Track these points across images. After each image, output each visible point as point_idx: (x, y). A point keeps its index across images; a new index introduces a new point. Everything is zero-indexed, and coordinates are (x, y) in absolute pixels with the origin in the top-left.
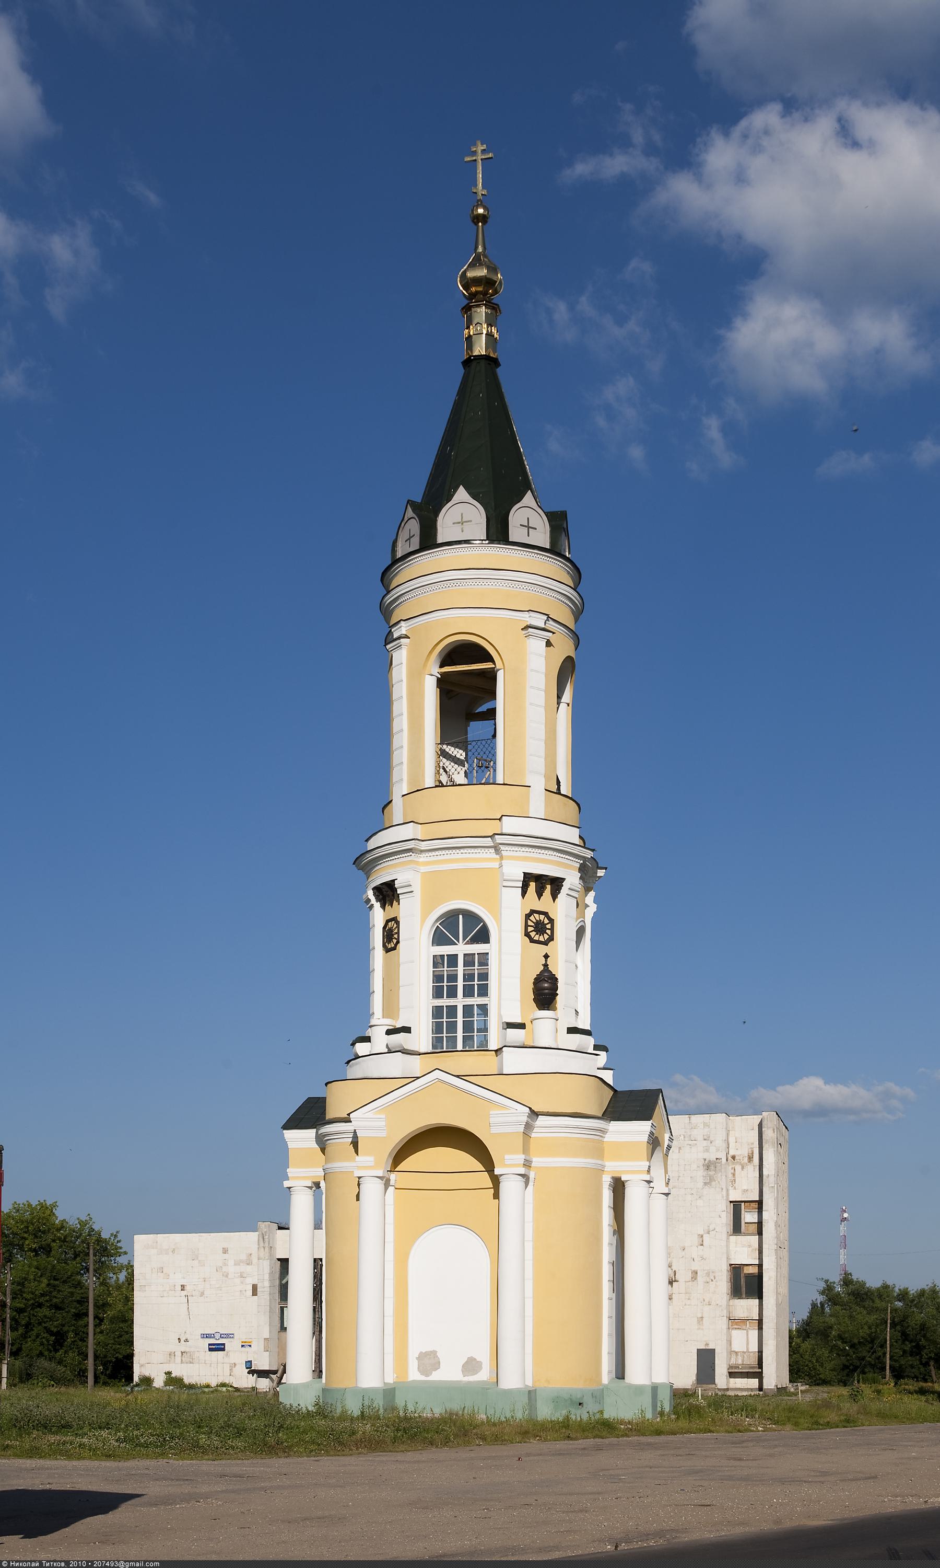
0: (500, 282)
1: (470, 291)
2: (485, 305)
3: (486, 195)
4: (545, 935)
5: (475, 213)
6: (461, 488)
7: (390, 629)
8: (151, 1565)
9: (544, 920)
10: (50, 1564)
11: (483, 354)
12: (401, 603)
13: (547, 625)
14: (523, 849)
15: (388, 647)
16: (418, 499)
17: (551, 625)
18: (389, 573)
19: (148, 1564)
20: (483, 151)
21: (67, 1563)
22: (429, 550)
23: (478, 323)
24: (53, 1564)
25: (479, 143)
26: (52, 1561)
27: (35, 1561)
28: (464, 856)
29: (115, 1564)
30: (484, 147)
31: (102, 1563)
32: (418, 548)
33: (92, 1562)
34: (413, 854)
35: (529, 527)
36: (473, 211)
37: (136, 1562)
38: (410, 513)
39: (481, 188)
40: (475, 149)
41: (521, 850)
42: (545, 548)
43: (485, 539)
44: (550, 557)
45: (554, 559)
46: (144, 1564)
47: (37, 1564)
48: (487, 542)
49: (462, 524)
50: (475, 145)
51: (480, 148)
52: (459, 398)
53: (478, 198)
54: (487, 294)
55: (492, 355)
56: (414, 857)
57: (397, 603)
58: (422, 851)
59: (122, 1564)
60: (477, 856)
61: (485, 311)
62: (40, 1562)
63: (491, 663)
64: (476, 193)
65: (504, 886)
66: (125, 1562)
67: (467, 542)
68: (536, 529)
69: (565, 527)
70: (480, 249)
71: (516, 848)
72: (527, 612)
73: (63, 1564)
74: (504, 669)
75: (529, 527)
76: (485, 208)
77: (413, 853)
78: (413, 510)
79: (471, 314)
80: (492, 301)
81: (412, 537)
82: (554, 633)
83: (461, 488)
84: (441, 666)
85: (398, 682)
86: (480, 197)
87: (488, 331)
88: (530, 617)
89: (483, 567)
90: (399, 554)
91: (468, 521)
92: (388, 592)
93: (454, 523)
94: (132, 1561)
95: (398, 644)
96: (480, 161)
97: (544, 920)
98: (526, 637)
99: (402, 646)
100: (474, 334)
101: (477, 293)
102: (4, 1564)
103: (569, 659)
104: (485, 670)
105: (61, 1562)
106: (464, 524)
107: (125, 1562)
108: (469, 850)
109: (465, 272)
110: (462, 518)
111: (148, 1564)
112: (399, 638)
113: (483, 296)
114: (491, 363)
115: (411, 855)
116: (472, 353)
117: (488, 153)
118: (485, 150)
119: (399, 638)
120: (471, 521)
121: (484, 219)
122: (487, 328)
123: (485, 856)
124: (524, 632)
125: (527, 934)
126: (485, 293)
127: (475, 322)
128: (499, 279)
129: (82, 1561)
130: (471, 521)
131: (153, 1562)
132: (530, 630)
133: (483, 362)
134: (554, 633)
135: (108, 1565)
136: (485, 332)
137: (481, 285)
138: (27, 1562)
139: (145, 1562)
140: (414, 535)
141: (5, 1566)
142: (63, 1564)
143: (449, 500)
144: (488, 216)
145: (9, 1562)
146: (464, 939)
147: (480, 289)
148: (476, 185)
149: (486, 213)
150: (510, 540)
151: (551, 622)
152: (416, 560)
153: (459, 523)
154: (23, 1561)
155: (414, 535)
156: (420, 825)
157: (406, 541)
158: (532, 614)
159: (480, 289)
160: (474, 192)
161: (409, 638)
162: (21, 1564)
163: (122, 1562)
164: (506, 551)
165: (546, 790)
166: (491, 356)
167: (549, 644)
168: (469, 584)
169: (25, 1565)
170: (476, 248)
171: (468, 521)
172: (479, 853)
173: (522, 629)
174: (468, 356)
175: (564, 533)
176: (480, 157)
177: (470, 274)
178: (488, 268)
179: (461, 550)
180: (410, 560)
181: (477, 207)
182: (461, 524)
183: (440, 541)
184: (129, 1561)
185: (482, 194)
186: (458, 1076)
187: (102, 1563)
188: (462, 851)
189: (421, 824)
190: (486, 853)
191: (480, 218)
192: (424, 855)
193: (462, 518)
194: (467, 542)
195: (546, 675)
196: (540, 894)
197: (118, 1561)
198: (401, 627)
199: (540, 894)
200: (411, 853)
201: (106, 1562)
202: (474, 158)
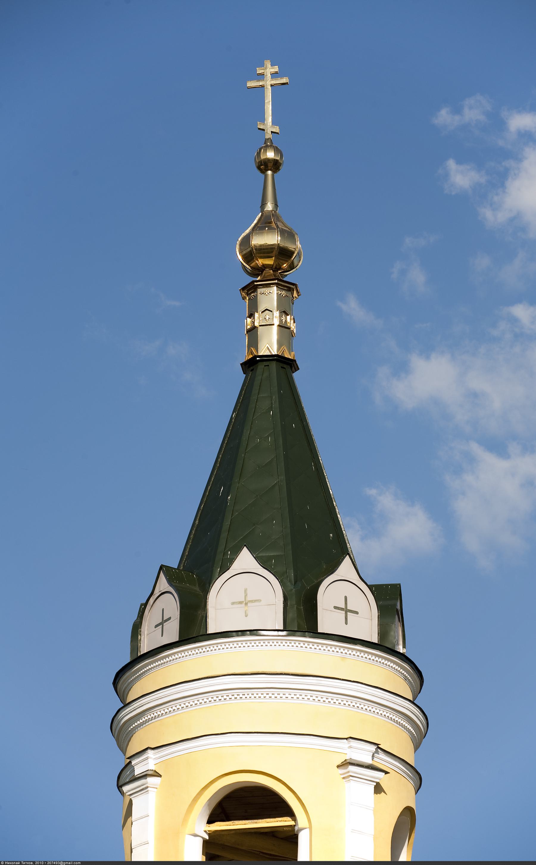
0: (299, 254)
1: (253, 264)
2: (277, 285)
3: (278, 133)
5: (263, 157)
6: (245, 551)
7: (128, 760)
8: (77, 863)
11: (274, 354)
12: (146, 721)
13: (375, 759)
15: (125, 789)
16: (174, 563)
17: (382, 760)
18: (128, 674)
19: (75, 863)
20: (274, 75)
21: (34, 862)
22: (195, 642)
23: (267, 310)
24: (27, 863)
25: (268, 63)
26: (26, 862)
27: (18, 862)
29: (58, 863)
30: (276, 69)
31: (52, 863)
32: (177, 639)
33: (46, 862)
35: (347, 611)
36: (259, 154)
38: (163, 584)
39: (271, 124)
40: (261, 72)
42: (372, 643)
43: (282, 628)
44: (379, 657)
45: (386, 659)
46: (73, 863)
47: (19, 863)
48: (284, 633)
49: (246, 604)
50: (262, 65)
51: (269, 69)
52: (237, 415)
53: (267, 137)
54: (280, 268)
55: (287, 355)
57: (141, 721)
59: (61, 863)
61: (277, 293)
62: (20, 862)
63: (289, 819)
64: (263, 130)
67: (253, 632)
69: (399, 607)
70: (269, 207)
72: (345, 740)
73: (32, 863)
74: (310, 828)
75: (347, 611)
76: (277, 150)
78: (170, 581)
79: (256, 297)
80: (285, 279)
81: (166, 620)
82: (386, 773)
83: (245, 551)
84: (210, 821)
85: (141, 845)
86: (269, 135)
87: (281, 321)
88: (350, 747)
89: (279, 671)
90: (144, 649)
91: (255, 601)
92: (126, 705)
93: (233, 603)
96: (270, 87)
98: (344, 778)
99: (149, 789)
100: (260, 326)
101: (265, 267)
102: (2, 863)
103: (408, 812)
104: (278, 829)
105: (31, 862)
106: (249, 604)
109: (247, 239)
110: (246, 596)
111: (75, 863)
112: (144, 776)
113: (273, 271)
114: (285, 366)
116: (257, 351)
117: (282, 77)
118: (276, 73)
119: (144, 776)
120: (259, 601)
121: (275, 165)
122: (281, 316)
126: (276, 268)
127: (261, 308)
128: (297, 250)
129: (41, 862)
130: (259, 601)
132: (351, 768)
133: (274, 365)
134: (386, 773)
136: (276, 322)
137: (272, 257)
138: (13, 862)
139: (73, 862)
140: (170, 619)
142: (32, 863)
143: (225, 568)
144: (281, 162)
145: (4, 862)
147: (270, 262)
148: (263, 120)
149: (278, 158)
150: (319, 631)
151: (382, 755)
152: (173, 657)
153: (241, 603)
154: (12, 862)
155: (170, 619)
157: (156, 626)
158: (354, 743)
159: (270, 262)
160: (259, 129)
161: (160, 776)
163: (62, 862)
164: (308, 647)
166: (286, 356)
167: (378, 789)
168: (257, 696)
169: (13, 863)
170: (263, 204)
171: (255, 601)
173: (338, 767)
174: (251, 356)
175: (397, 616)
176: (268, 82)
177: (258, 241)
178: (283, 233)
179: (240, 645)
180: (165, 657)
181: (266, 147)
182: (243, 605)
183: (211, 630)
184: (65, 862)
185: (272, 132)
187: (52, 863)
190: (249, 646)
191: (270, 165)
193: (246, 596)
194: (253, 632)
195: (375, 838)
197: (60, 862)
198: (147, 759)
201: (54, 862)
202: (261, 83)
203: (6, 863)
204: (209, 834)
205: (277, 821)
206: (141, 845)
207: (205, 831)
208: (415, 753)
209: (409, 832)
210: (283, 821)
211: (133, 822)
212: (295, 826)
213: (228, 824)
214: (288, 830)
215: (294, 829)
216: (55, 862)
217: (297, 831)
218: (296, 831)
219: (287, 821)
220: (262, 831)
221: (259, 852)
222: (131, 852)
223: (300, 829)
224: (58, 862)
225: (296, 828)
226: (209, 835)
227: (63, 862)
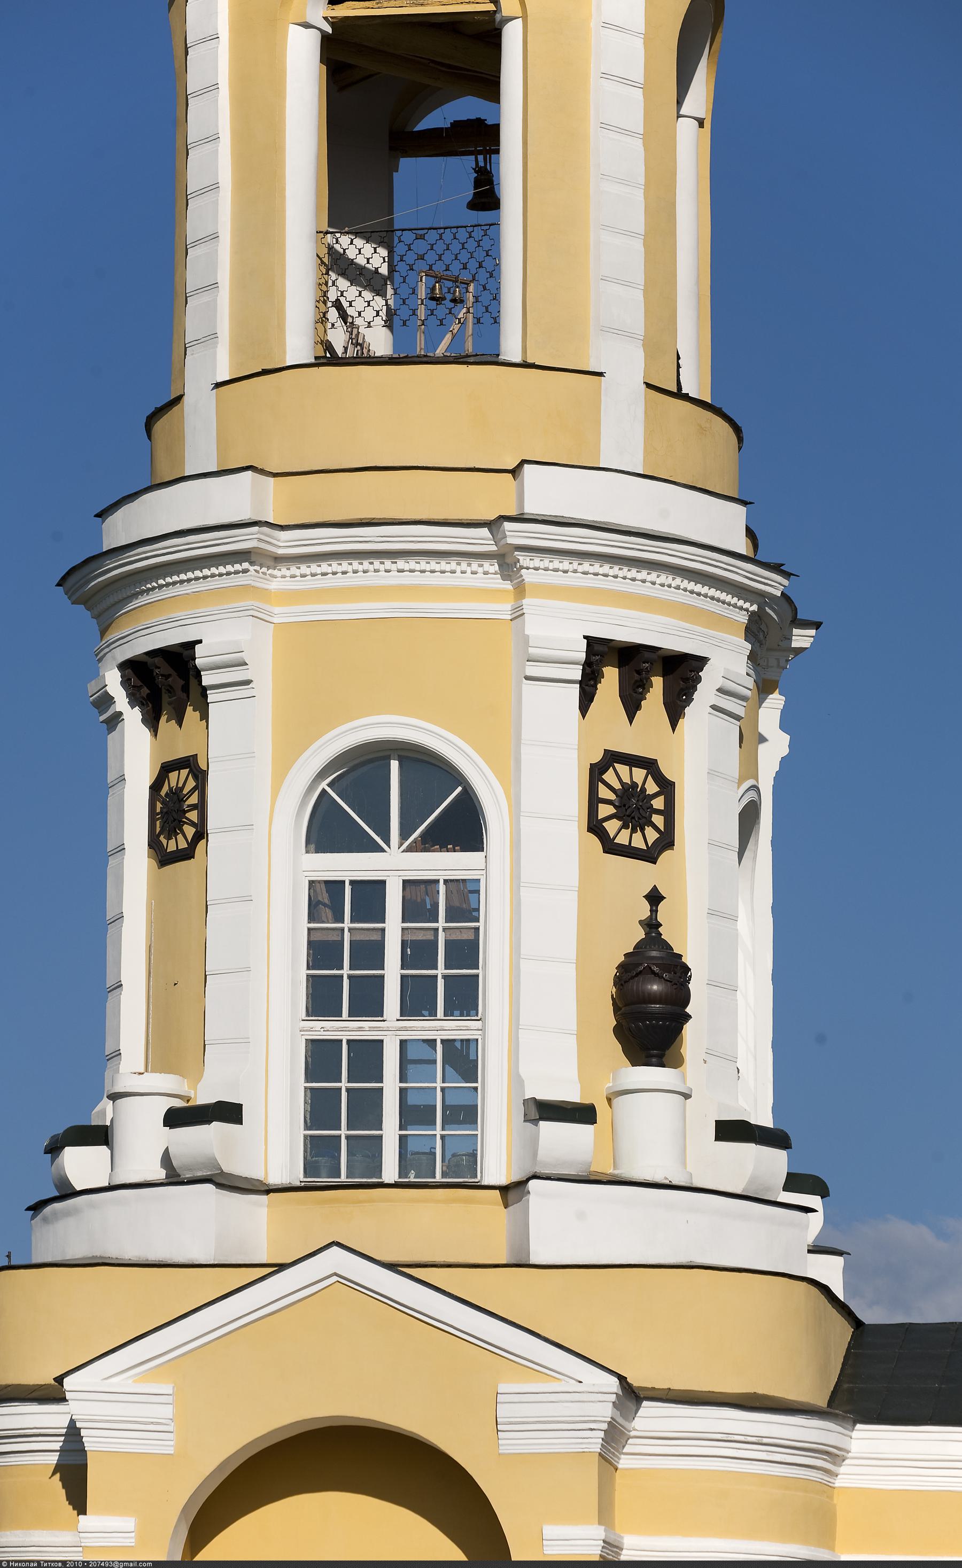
8: (145, 1565)
10: (48, 1565)
19: (141, 1565)
24: (51, 1564)
28: (407, 579)
29: (109, 1564)
31: (98, 1564)
33: (88, 1562)
34: (251, 568)
46: (138, 1564)
47: (36, 1565)
60: (447, 580)
73: (60, 1565)
74: (525, 18)
77: (252, 563)
85: (204, 40)
102: (4, 1564)
111: (141, 1565)
115: (245, 571)
123: (468, 581)
125: (595, 827)
135: (103, 1565)
139: (138, 1562)
141: (4, 1566)
146: (404, 836)
163: (117, 1563)
165: (648, 386)
169: (24, 1565)
172: (453, 572)
186: (392, 1267)
187: (98, 1564)
196: (632, 705)
199: (632, 705)
200: (246, 565)
203: (12, 1565)
204: (332, 22)
205: (462, 3)
206: (204, 40)
207: (326, 18)
208: (740, 747)
209: (711, 29)
210: (473, 3)
211: (189, 47)
212: (495, 12)
213: (368, 6)
214: (483, 19)
215: (494, 19)
216: (105, 1561)
217: (500, 21)
218: (497, 23)
219: (480, 3)
220: (434, 20)
221: (429, 60)
222: (187, 53)
223: (504, 18)
224: (109, 1561)
225: (498, 17)
226: (333, 25)
227: (119, 1562)
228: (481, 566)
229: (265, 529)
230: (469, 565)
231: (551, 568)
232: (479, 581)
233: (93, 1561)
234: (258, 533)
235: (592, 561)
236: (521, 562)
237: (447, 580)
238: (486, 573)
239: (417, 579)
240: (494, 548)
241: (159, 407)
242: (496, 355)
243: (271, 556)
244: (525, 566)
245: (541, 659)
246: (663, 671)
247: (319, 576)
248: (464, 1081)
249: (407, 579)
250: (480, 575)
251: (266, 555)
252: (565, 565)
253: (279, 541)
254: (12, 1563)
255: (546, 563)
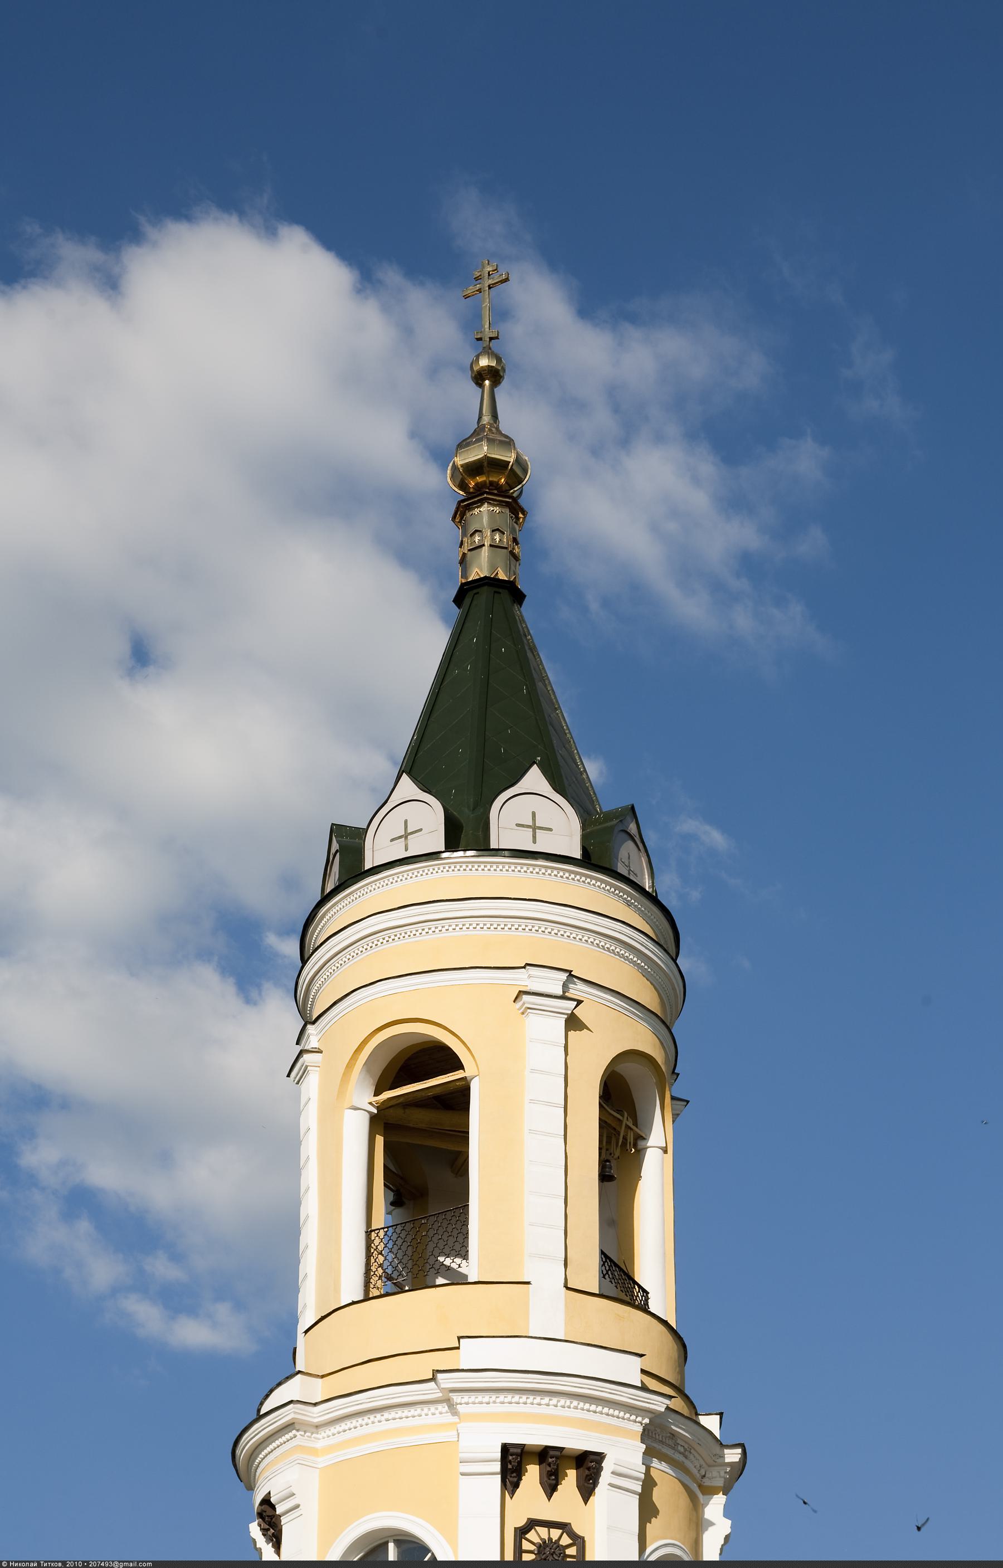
4: (537, 1540)
8: (144, 1565)
9: (539, 1536)
10: (48, 1564)
14: (502, 1397)
19: (141, 1565)
21: (64, 1563)
24: (51, 1564)
26: (49, 1562)
27: (33, 1562)
28: (392, 1425)
29: (109, 1564)
31: (98, 1564)
33: (88, 1562)
34: (298, 1434)
37: (129, 1562)
41: (498, 1400)
46: (138, 1564)
56: (298, 1439)
58: (318, 1427)
59: (116, 1565)
60: (417, 1422)
62: (39, 1562)
65: (462, 1474)
66: (119, 1562)
68: (550, 830)
71: (486, 1398)
73: (60, 1565)
77: (298, 1430)
84: (376, 1094)
88: (530, 977)
94: (126, 1562)
95: (303, 1066)
97: (539, 1536)
102: (4, 1564)
105: (58, 1562)
107: (119, 1562)
108: (400, 1413)
111: (141, 1565)
115: (295, 1436)
123: (431, 1420)
124: (519, 1004)
129: (78, 1562)
131: (146, 1562)
138: (25, 1562)
139: (138, 1562)
142: (60, 1565)
145: (8, 1562)
154: (22, 1562)
156: (320, 1380)
162: (20, 1564)
163: (117, 1563)
169: (24, 1565)
172: (420, 1416)
184: (123, 1562)
187: (98, 1564)
188: (387, 1415)
189: (323, 1377)
192: (323, 1433)
197: (113, 1562)
200: (294, 1432)
201: (101, 1562)
216: (105, 1562)
224: (109, 1562)
228: (437, 1409)
229: (299, 1406)
230: (429, 1409)
231: (477, 1402)
232: (438, 1419)
233: (70, 1561)
234: (294, 1408)
235: (505, 1394)
236: (455, 1400)
237: (417, 1422)
238: (441, 1413)
239: (398, 1424)
240: (440, 1395)
241: (658, 898)
242: (492, 287)
243: (311, 1425)
244: (458, 1402)
245: (469, 1460)
246: (539, 1461)
247: (342, 1433)
248: (711, 1496)
249: (392, 1425)
250: (438, 1415)
251: (308, 1425)
252: (486, 1399)
253: (313, 1413)
254: (12, 1563)
255: (473, 1399)
